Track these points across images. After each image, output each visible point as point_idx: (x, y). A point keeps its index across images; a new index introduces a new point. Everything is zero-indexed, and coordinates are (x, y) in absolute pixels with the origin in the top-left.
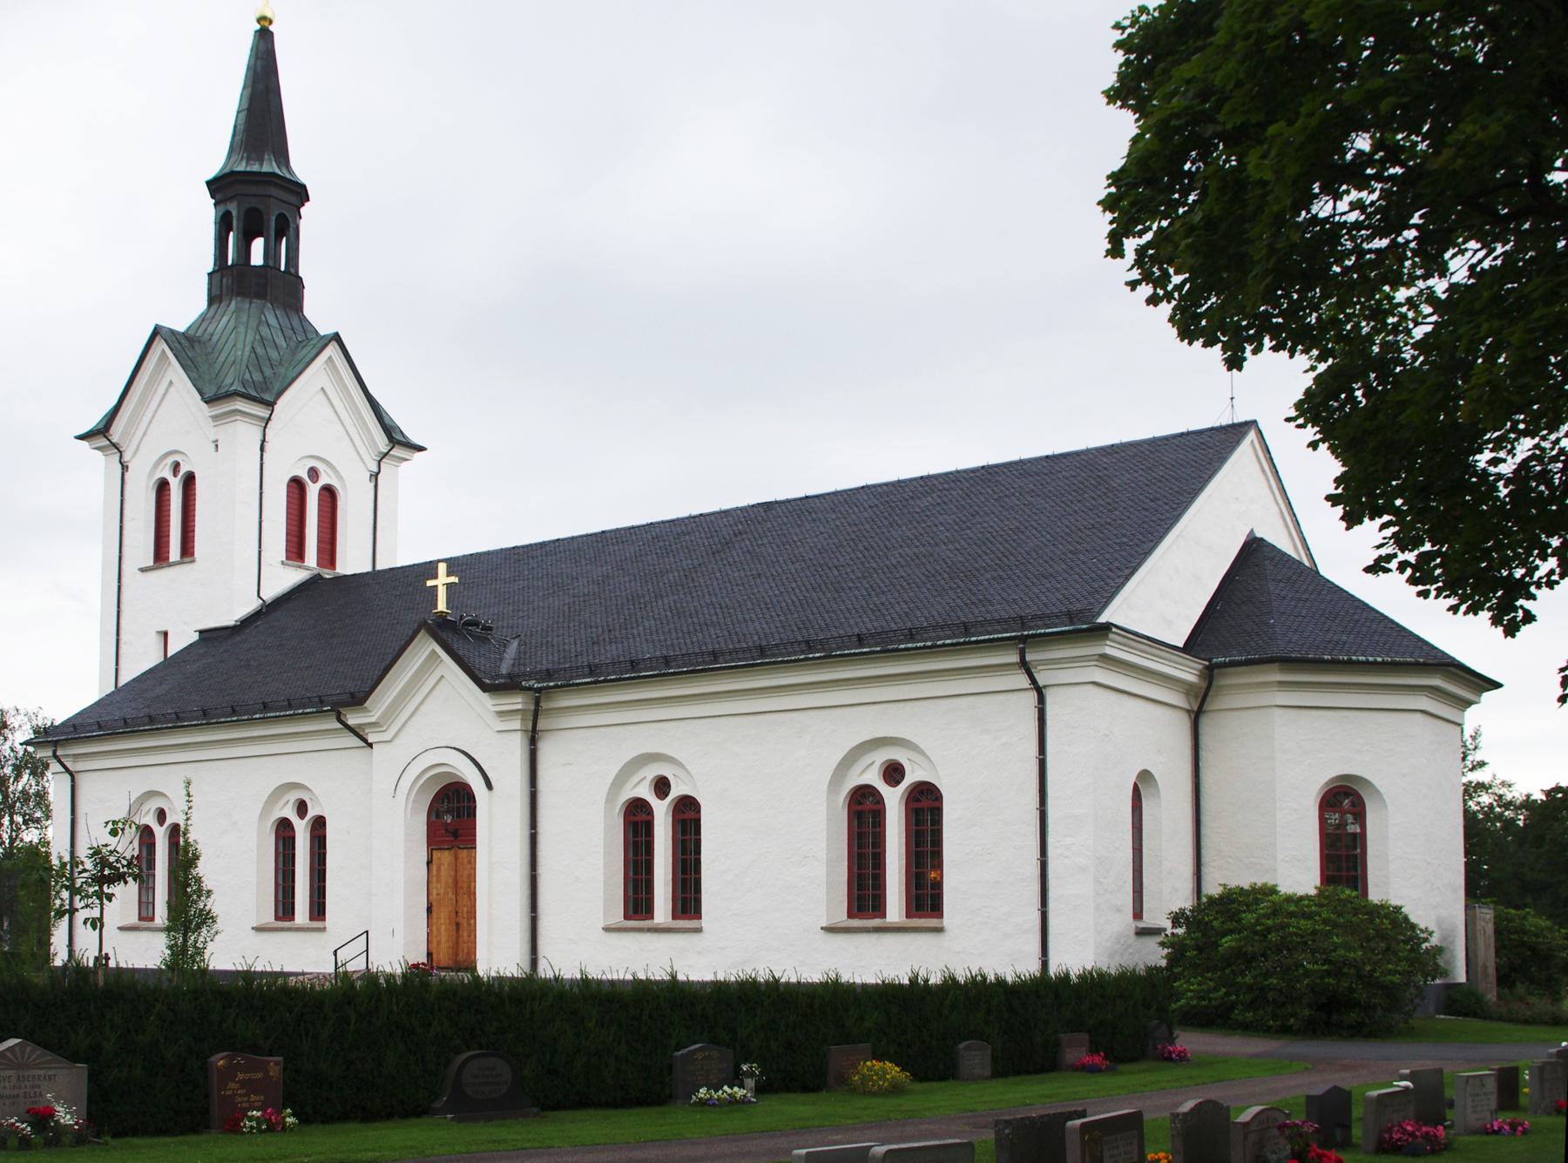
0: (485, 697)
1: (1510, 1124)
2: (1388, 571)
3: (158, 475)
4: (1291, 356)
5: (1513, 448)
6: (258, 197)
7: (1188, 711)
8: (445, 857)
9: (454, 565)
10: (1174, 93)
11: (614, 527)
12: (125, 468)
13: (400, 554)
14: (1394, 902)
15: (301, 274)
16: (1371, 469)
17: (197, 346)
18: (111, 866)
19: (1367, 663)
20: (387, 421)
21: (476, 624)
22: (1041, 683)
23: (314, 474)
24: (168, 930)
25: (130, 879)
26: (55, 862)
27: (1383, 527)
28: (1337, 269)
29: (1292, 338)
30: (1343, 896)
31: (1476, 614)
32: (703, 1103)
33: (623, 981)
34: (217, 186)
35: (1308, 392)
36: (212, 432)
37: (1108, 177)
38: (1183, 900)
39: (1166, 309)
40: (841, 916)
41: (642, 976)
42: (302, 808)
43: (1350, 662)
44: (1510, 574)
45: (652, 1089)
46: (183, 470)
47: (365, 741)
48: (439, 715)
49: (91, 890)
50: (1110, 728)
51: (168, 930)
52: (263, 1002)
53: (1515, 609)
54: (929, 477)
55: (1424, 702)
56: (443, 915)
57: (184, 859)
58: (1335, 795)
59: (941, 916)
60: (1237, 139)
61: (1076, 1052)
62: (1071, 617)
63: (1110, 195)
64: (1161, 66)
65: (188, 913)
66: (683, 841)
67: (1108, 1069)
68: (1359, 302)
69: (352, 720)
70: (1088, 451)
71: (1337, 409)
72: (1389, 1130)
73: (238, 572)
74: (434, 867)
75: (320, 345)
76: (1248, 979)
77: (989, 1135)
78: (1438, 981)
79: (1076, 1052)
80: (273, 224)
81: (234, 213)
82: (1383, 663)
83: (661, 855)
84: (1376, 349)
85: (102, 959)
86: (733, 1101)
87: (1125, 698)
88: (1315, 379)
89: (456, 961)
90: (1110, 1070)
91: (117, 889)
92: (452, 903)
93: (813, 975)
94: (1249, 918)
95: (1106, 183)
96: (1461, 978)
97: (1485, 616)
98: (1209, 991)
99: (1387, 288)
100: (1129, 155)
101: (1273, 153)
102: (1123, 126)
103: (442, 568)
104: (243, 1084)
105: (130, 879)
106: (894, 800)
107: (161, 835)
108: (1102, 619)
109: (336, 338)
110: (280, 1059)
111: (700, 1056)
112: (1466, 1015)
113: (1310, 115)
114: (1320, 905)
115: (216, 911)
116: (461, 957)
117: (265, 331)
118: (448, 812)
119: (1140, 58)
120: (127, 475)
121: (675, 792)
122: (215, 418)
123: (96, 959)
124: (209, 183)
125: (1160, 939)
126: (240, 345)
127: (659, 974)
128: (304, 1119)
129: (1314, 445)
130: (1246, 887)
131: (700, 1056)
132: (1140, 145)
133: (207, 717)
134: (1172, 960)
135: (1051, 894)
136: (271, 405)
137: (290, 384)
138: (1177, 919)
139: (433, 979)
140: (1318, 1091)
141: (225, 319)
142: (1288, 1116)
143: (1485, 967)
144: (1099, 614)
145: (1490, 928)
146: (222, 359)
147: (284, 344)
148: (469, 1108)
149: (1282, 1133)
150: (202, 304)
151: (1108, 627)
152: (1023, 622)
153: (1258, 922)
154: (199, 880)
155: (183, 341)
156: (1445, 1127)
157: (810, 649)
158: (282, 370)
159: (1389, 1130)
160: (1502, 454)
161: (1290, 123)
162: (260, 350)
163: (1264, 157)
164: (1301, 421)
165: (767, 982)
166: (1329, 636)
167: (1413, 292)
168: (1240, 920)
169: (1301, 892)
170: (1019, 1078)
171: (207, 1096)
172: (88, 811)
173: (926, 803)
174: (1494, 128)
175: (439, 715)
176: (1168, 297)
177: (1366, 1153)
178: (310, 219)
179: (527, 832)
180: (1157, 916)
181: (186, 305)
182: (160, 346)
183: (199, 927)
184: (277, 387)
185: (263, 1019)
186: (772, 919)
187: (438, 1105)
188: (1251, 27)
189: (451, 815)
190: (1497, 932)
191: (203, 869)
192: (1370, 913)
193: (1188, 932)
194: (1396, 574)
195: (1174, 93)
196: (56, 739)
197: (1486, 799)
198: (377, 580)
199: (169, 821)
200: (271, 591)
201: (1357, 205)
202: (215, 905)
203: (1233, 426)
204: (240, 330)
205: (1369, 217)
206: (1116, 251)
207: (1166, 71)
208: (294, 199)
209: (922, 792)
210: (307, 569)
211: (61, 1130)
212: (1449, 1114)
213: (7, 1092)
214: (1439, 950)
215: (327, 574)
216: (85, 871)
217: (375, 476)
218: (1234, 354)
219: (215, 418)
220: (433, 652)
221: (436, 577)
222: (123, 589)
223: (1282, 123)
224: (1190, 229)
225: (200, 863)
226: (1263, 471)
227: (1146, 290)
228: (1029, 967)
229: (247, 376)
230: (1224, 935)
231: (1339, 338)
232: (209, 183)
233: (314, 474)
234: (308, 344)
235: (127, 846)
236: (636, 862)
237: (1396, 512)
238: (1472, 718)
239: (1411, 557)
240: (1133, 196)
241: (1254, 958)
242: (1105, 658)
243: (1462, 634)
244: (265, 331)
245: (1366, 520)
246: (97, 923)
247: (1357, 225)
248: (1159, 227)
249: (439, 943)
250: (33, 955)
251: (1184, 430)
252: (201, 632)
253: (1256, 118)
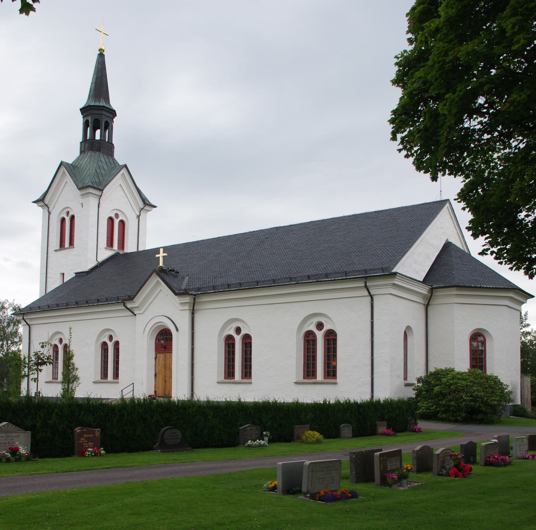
0: (176, 297)
1: (532, 456)
2: (487, 254)
3: (62, 216)
4: (455, 177)
5: (534, 211)
6: (98, 115)
7: (424, 305)
8: (161, 356)
9: (166, 249)
10: (415, 82)
11: (182, 243)
12: (49, 213)
13: (148, 245)
14: (495, 375)
16: (481, 218)
17: (76, 169)
18: (41, 359)
19: (487, 288)
20: (143, 197)
21: (173, 271)
22: (372, 294)
23: (117, 216)
24: (62, 383)
25: (48, 364)
26: (23, 358)
27: (486, 239)
28: (472, 145)
29: (455, 171)
30: (477, 373)
31: (519, 270)
32: (249, 446)
33: (222, 401)
34: (84, 110)
35: (462, 190)
36: (81, 200)
37: (392, 112)
38: (422, 373)
39: (411, 159)
40: (301, 378)
41: (229, 400)
42: (111, 338)
43: (481, 287)
44: (531, 256)
45: (231, 441)
46: (70, 214)
47: (133, 313)
48: (160, 305)
49: (34, 368)
50: (397, 311)
51: (62, 383)
52: (95, 410)
53: (533, 269)
54: (334, 218)
55: (507, 302)
56: (160, 377)
57: (68, 357)
58: (475, 336)
59: (336, 378)
60: (437, 98)
61: (382, 428)
62: (383, 270)
63: (392, 118)
64: (411, 72)
65: (69, 377)
66: (246, 351)
67: (394, 435)
68: (480, 158)
69: (129, 306)
70: (390, 210)
71: (472, 196)
72: (489, 457)
73: (90, 251)
74: (157, 360)
75: (119, 169)
76: (444, 402)
77: (348, 458)
78: (510, 404)
79: (382, 428)
80: (103, 125)
81: (90, 121)
82: (493, 288)
83: (238, 356)
84: (486, 175)
85: (38, 393)
86: (260, 446)
87: (401, 299)
88: (465, 185)
89: (165, 394)
90: (394, 435)
91: (44, 367)
92: (163, 374)
93: (289, 400)
94: (444, 380)
95: (391, 114)
96: (519, 403)
97: (522, 271)
98: (430, 407)
99: (490, 153)
100: (399, 104)
101: (448, 104)
102: (398, 92)
103: (161, 250)
104: (86, 438)
105: (48, 364)
106: (320, 336)
107: (61, 348)
108: (394, 271)
109: (126, 166)
110: (99, 429)
111: (248, 429)
112: (521, 416)
113: (460, 91)
114: (469, 376)
115: (79, 376)
116: (167, 393)
117: (100, 164)
118: (163, 339)
119: (404, 69)
120: (50, 216)
121: (326, 328)
122: (82, 195)
123: (36, 393)
124: (81, 110)
125: (413, 387)
126: (91, 169)
127: (235, 399)
128: (108, 451)
129: (464, 209)
130: (443, 369)
131: (248, 429)
132: (403, 100)
133: (78, 305)
134: (417, 395)
135: (375, 371)
136: (102, 190)
137: (109, 183)
138: (419, 380)
139: (155, 401)
140: (465, 443)
141: (86, 159)
142: (453, 452)
143: (527, 399)
144: (393, 269)
145: (529, 385)
146: (85, 173)
147: (107, 168)
148: (166, 448)
149: (451, 458)
150: (78, 154)
151: (395, 274)
152: (366, 271)
153: (447, 382)
154: (73, 364)
155: (71, 167)
156: (509, 457)
157: (291, 280)
158: (106, 178)
159: (489, 457)
160: (530, 213)
161: (454, 94)
162: (98, 171)
163: (445, 105)
164: (459, 200)
165: (273, 402)
166: (474, 278)
167: (500, 154)
168: (441, 381)
169: (462, 371)
170: (362, 438)
171: (73, 443)
172: (32, 339)
173: (331, 337)
174: (524, 96)
175: (160, 305)
176: (412, 155)
177: (481, 465)
178: (117, 123)
179: (190, 347)
180: (412, 379)
181: (72, 154)
182: (63, 169)
183: (73, 381)
184: (104, 184)
185: (93, 415)
186: (276, 380)
187: (155, 446)
188: (440, 59)
189: (164, 340)
190: (531, 386)
191: (75, 360)
192: (486, 379)
193: (423, 385)
194: (489, 256)
195: (415, 82)
196: (23, 313)
197: (529, 338)
198: (139, 254)
199: (64, 343)
200: (101, 259)
201: (480, 123)
202: (79, 373)
203: (441, 201)
204: (93, 161)
205: (484, 127)
206: (394, 138)
207: (412, 74)
208: (111, 116)
209: (330, 333)
210: (114, 250)
211: (21, 456)
212: (511, 452)
213: (2, 442)
214: (511, 392)
215: (121, 252)
216: (32, 361)
217: (138, 217)
218: (435, 175)
219: (82, 195)
220: (158, 281)
221: (159, 253)
222: (49, 258)
223: (451, 94)
224: (419, 131)
225: (74, 358)
226: (451, 218)
227: (404, 152)
228: (367, 397)
229: (94, 180)
230: (436, 386)
231: (473, 171)
232: (81, 110)
233: (117, 216)
234: (115, 168)
235: (47, 352)
236: (229, 358)
237: (490, 233)
238: (524, 308)
239: (495, 250)
240: (401, 118)
241: (446, 395)
242: (394, 285)
243: (517, 278)
244: (100, 164)
245: (480, 236)
246: (36, 380)
247: (479, 130)
248: (410, 131)
249: (159, 388)
250: (15, 392)
251: (424, 202)
252: (76, 273)
253: (442, 91)
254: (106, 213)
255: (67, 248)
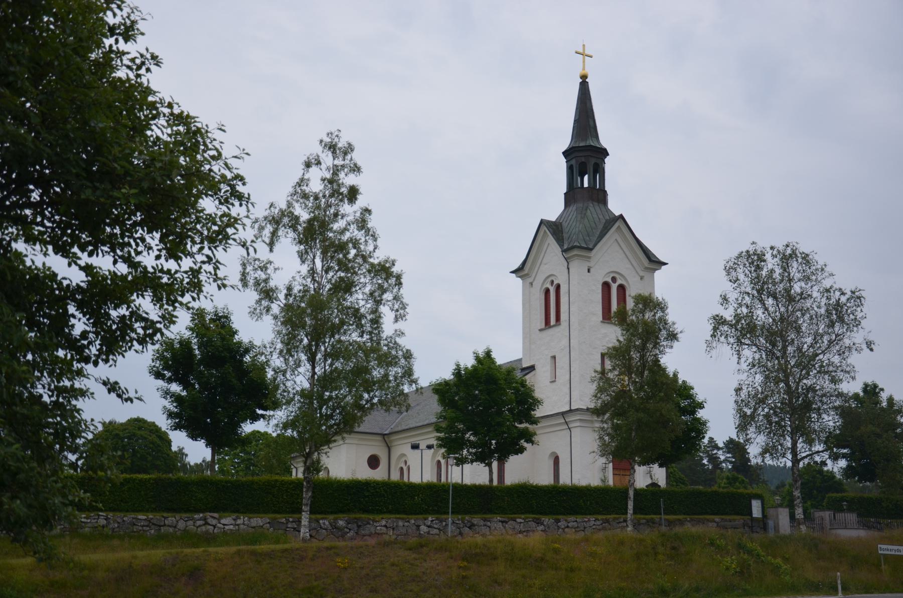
3: (545, 287)
6: (586, 157)
15: (606, 189)
23: (614, 280)
34: (566, 154)
46: (555, 283)
109: (621, 217)
124: (564, 153)
178: (610, 165)
182: (544, 228)
228: (386, 478)
232: (564, 153)
233: (614, 280)
254: (600, 275)
255: (554, 326)
